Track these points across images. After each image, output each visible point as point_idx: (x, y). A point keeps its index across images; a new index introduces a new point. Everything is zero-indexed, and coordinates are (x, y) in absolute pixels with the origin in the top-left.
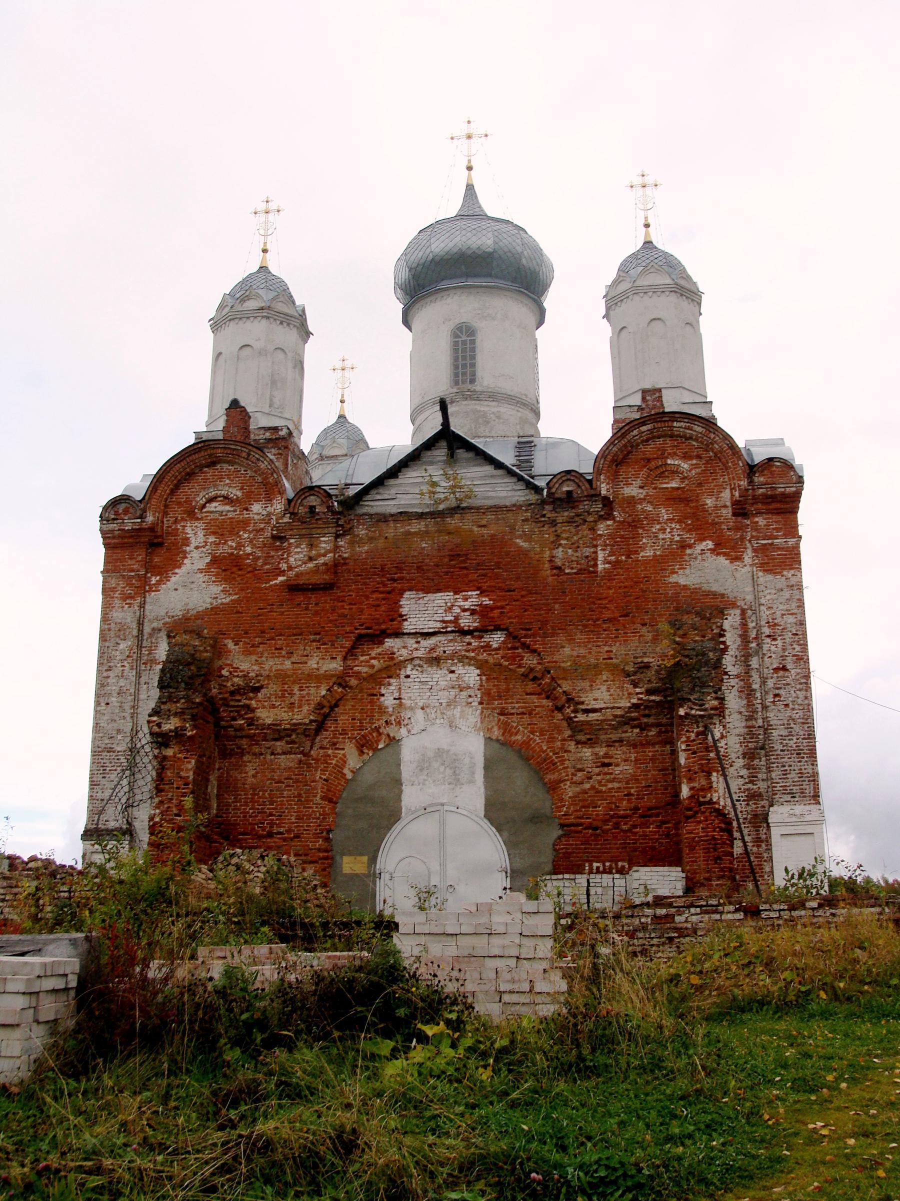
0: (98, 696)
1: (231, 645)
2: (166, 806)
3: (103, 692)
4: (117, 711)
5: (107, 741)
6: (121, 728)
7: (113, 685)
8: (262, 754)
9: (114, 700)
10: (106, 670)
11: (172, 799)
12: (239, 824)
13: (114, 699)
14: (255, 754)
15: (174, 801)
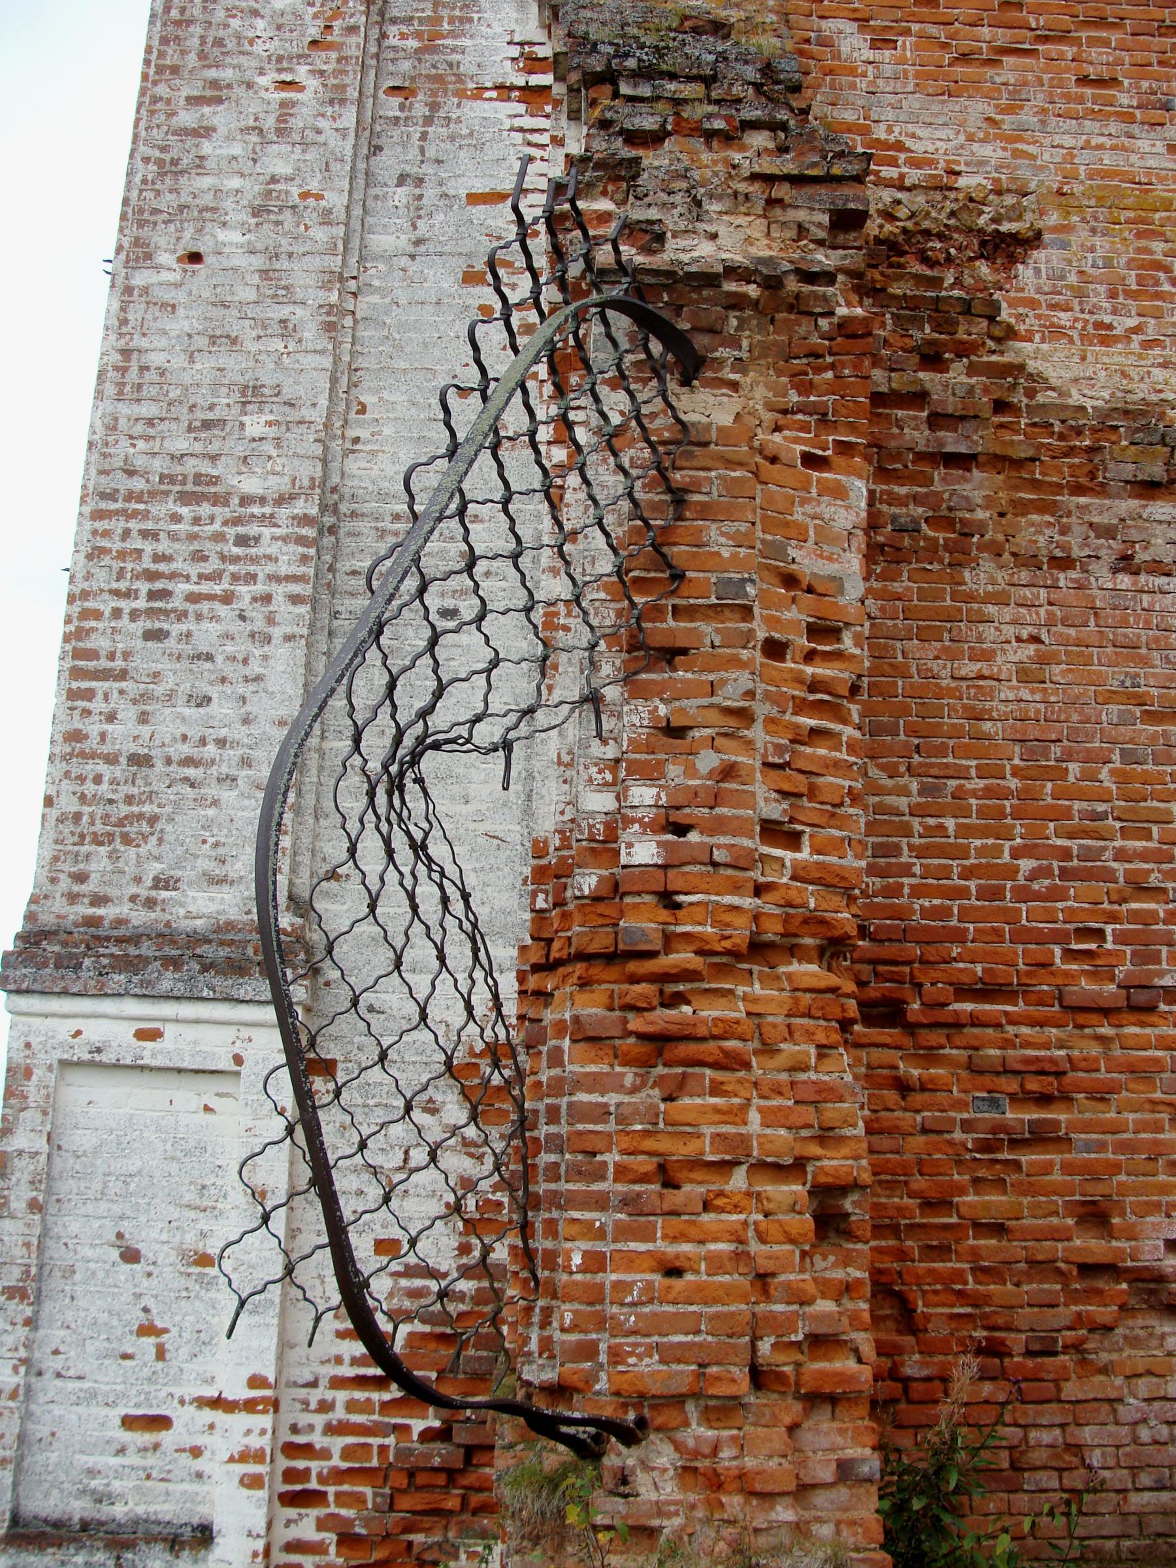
0: (137, 216)
1: (852, 43)
2: (707, 761)
3: (168, 201)
4: (250, 294)
5: (181, 444)
6: (267, 376)
7: (229, 162)
8: (1064, 563)
9: (229, 239)
10: (194, 101)
11: (744, 716)
12: (959, 936)
13: (232, 236)
14: (1030, 561)
15: (757, 733)
